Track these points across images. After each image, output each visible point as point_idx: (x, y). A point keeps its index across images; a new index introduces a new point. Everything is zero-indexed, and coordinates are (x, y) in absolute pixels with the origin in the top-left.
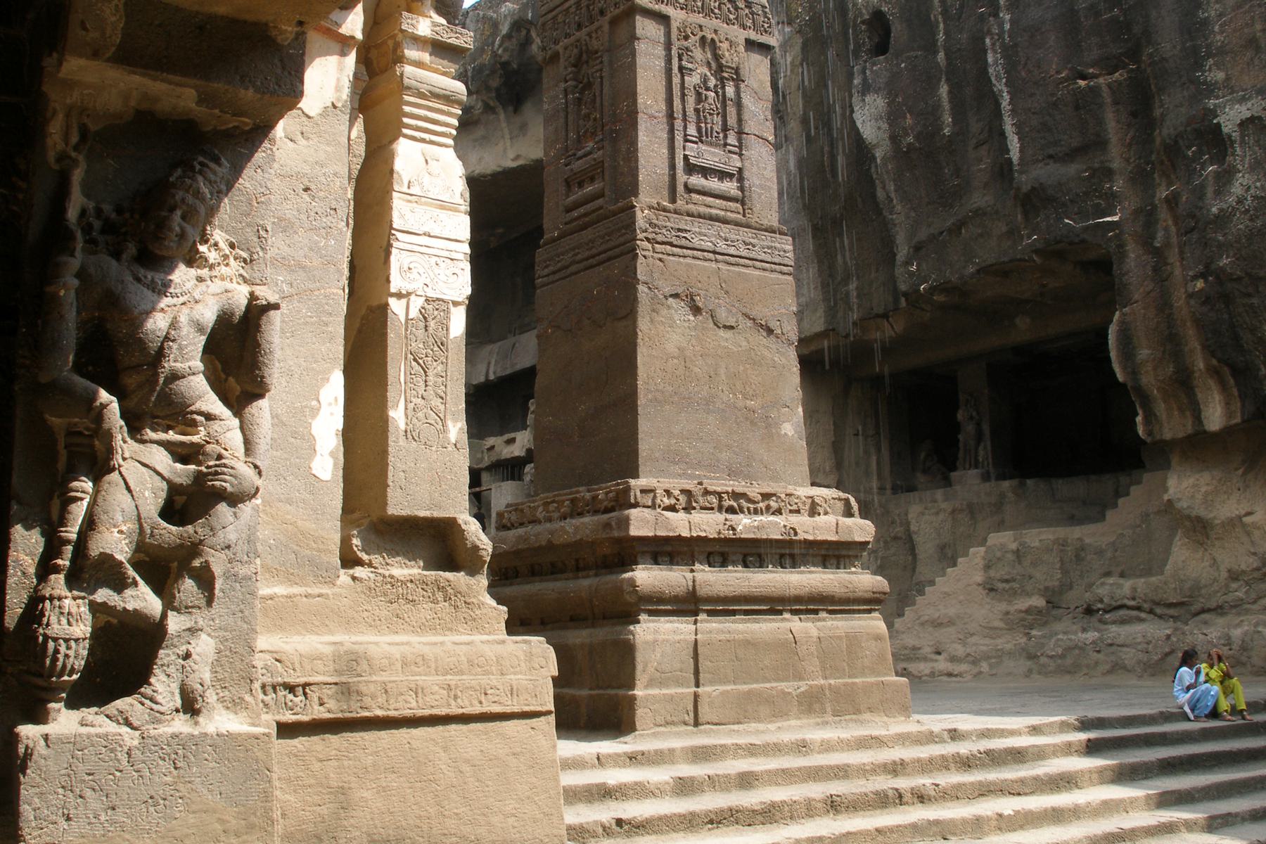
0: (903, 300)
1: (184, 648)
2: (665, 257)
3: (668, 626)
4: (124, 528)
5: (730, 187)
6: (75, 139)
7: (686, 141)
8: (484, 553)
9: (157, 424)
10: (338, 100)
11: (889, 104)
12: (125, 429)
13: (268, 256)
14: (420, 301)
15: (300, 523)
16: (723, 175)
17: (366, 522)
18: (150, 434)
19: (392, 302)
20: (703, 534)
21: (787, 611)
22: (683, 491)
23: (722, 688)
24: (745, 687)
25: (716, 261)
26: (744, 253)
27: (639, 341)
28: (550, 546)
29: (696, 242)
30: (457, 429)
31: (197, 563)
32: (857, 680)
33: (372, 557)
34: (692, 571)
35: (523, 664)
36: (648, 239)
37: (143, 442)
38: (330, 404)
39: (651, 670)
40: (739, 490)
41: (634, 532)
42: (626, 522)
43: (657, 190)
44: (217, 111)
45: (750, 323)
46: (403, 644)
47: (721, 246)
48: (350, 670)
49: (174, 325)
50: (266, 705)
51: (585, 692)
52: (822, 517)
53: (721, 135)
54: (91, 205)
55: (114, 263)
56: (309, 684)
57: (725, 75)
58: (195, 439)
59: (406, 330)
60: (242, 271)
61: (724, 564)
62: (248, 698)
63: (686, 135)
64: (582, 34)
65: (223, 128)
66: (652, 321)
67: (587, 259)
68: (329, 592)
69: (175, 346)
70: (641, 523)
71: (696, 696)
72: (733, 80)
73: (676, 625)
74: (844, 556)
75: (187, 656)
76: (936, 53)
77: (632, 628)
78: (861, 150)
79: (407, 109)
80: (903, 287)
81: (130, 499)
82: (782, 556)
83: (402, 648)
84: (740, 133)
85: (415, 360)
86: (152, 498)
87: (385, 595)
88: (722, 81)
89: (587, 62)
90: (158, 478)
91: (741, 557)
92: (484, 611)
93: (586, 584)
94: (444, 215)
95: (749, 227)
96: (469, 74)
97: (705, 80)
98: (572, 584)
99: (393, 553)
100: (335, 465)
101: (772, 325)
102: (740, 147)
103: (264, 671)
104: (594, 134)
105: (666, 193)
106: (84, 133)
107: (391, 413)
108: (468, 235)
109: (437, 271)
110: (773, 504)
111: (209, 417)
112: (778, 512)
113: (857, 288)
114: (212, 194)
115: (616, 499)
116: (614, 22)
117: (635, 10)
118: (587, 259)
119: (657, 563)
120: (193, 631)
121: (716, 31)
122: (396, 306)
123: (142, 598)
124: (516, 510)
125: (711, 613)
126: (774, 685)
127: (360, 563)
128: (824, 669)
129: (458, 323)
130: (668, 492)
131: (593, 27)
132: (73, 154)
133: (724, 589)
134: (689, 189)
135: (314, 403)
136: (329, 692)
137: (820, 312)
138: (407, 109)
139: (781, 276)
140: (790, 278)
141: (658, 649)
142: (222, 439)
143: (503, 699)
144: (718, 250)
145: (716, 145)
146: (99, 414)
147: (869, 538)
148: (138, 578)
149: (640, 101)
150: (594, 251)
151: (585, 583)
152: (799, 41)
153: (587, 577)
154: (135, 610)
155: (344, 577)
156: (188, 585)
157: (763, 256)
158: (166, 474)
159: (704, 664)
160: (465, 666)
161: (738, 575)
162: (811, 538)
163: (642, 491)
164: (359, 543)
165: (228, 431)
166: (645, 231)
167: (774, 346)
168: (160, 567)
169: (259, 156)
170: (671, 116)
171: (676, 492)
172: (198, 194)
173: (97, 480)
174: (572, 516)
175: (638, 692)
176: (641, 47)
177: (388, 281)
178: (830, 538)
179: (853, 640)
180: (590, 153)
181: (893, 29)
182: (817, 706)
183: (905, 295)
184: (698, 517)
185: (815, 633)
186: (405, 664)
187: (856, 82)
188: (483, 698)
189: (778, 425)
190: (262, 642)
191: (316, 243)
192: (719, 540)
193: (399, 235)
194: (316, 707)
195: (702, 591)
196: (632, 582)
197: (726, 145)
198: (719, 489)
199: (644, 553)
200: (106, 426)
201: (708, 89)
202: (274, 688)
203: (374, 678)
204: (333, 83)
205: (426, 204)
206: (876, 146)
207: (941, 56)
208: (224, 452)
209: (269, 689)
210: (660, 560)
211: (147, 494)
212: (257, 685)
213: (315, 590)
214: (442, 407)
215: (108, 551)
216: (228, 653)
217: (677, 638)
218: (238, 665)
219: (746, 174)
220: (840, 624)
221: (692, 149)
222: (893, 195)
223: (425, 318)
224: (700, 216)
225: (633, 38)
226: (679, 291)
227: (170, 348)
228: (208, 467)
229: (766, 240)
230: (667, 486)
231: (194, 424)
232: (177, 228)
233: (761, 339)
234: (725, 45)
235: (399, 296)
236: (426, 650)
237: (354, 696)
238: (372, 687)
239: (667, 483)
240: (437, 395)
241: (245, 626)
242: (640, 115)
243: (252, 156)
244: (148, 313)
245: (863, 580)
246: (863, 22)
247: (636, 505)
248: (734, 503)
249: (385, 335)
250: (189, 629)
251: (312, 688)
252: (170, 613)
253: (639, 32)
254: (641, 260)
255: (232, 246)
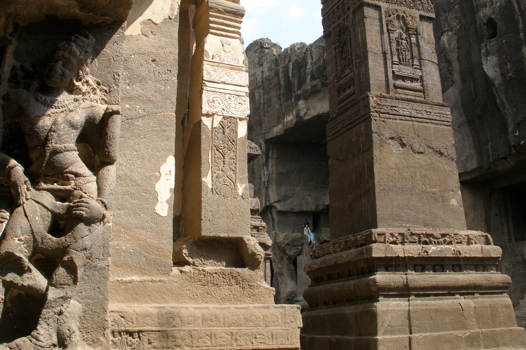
0: (513, 149)
1: (59, 308)
2: (385, 120)
3: (394, 302)
4: (22, 238)
5: (417, 85)
6: (10, 30)
7: (393, 64)
8: (259, 257)
9: (47, 179)
10: (172, 15)
11: (499, 60)
12: (29, 182)
13: (120, 89)
14: (220, 118)
15: (148, 240)
16: (413, 80)
17: (191, 241)
18: (43, 185)
19: (204, 119)
20: (411, 255)
21: (457, 294)
22: (400, 234)
23: (424, 334)
24: (436, 334)
25: (412, 121)
26: (426, 117)
27: (375, 161)
28: (336, 265)
29: (401, 112)
30: (242, 187)
31: (66, 258)
32: (497, 329)
33: (195, 260)
34: (406, 274)
35: (280, 321)
36: (376, 112)
37: (39, 190)
38: (167, 174)
39: (385, 325)
40: (429, 232)
41: (374, 255)
42: (370, 250)
43: (380, 88)
44: (92, 14)
45: (431, 151)
46: (204, 308)
47: (414, 114)
48: (169, 323)
49: (55, 123)
50: (115, 343)
51: (353, 338)
52: (474, 245)
53: (410, 61)
54: (18, 64)
55: (25, 92)
56: (142, 331)
57: (411, 32)
58: (68, 187)
59: (212, 134)
60: (104, 97)
61: (423, 270)
62: (102, 339)
63: (392, 61)
64: (341, 21)
65: (96, 23)
66: (381, 151)
67: (349, 125)
68: (166, 279)
69: (55, 135)
70: (378, 251)
71: (410, 339)
72: (415, 34)
73: (398, 302)
74: (487, 265)
75: (61, 313)
76: (519, 33)
77: (375, 304)
78: (488, 81)
79: (212, 19)
80: (512, 143)
81: (26, 221)
82: (453, 266)
83: (202, 311)
84: (420, 59)
85: (217, 150)
86: (41, 221)
87: (200, 281)
88: (409, 35)
89: (344, 33)
90: (44, 209)
91: (432, 267)
92: (260, 290)
93: (352, 283)
94: (233, 73)
95: (426, 104)
96: (315, 70)
97: (401, 35)
98: (346, 283)
99: (207, 258)
100: (169, 208)
101: (443, 151)
102: (420, 66)
103: (114, 323)
104: (349, 66)
105: (384, 89)
106: (16, 27)
107: (203, 179)
108: (247, 82)
109: (229, 102)
110: (447, 239)
111: (77, 175)
112: (450, 243)
113: (491, 146)
114: (81, 53)
115: (366, 239)
116: (354, 12)
117: (364, 4)
118: (349, 125)
119: (387, 271)
120: (65, 299)
121: (404, 12)
122: (205, 121)
123: (36, 279)
124: (321, 249)
125: (417, 296)
126: (452, 332)
127: (188, 263)
128: (478, 323)
129: (242, 130)
130: (392, 235)
131: (345, 16)
132: (9, 38)
133: (423, 283)
134: (395, 87)
135: (157, 174)
136: (155, 336)
137: (475, 159)
138: (212, 19)
139: (445, 127)
140: (450, 128)
141: (389, 315)
142: (83, 187)
143: (267, 341)
144: (412, 115)
145: (408, 66)
146: (8, 172)
147: (499, 255)
148: (32, 267)
149: (368, 46)
150: (352, 120)
151: (352, 282)
152: (455, 38)
153: (354, 279)
154: (29, 286)
155: (175, 270)
156: (61, 271)
157: (435, 118)
158: (50, 207)
159: (414, 322)
160: (243, 321)
161: (430, 276)
162: (468, 256)
163: (379, 235)
164: (187, 252)
165: (89, 182)
166: (375, 108)
167: (444, 161)
168: (48, 261)
169: (116, 37)
170: (384, 54)
171: (396, 235)
172: (71, 52)
173: (11, 213)
174: (346, 250)
175: (379, 337)
176: (367, 21)
177: (201, 108)
178: (478, 256)
179: (493, 308)
180: (347, 75)
181: (498, 25)
182: (475, 343)
183: (514, 146)
184: (407, 246)
185: (472, 305)
186: (204, 320)
187: (482, 51)
188: (254, 340)
189: (448, 200)
190: (112, 306)
191: (159, 88)
192: (419, 258)
193: (207, 83)
194: (146, 345)
195: (412, 284)
196: (374, 281)
197: (413, 65)
198: (418, 232)
199: (380, 265)
200: (13, 179)
201: (402, 39)
202: (120, 333)
203: (184, 328)
204: (169, 6)
205: (222, 67)
206: (495, 79)
207: (522, 34)
208: (84, 194)
209: (117, 334)
210: (389, 269)
211: (37, 218)
212: (108, 332)
213: (158, 278)
214: (234, 176)
215: (11, 251)
216: (90, 312)
217: (399, 308)
218: (97, 319)
219: (424, 78)
220: (486, 300)
221: (396, 68)
222: (504, 101)
223: (223, 127)
224: (402, 100)
225: (364, 17)
226: (394, 136)
227: (52, 135)
228: (75, 203)
229: (437, 110)
230: (391, 232)
231: (68, 179)
232: (59, 71)
233: (436, 158)
234: (409, 19)
235: (207, 115)
236: (218, 312)
237: (171, 339)
238: (182, 333)
239: (391, 230)
240: (231, 169)
241: (101, 296)
242: (369, 53)
243: (112, 36)
244: (40, 117)
245: (498, 277)
246: (484, 24)
247: (375, 242)
248: (427, 239)
249: (200, 137)
250: (62, 297)
251: (144, 333)
252: (50, 288)
253: (366, 14)
254: (373, 121)
255: (98, 84)
